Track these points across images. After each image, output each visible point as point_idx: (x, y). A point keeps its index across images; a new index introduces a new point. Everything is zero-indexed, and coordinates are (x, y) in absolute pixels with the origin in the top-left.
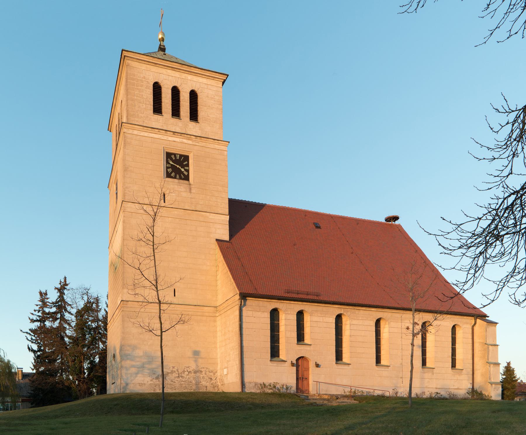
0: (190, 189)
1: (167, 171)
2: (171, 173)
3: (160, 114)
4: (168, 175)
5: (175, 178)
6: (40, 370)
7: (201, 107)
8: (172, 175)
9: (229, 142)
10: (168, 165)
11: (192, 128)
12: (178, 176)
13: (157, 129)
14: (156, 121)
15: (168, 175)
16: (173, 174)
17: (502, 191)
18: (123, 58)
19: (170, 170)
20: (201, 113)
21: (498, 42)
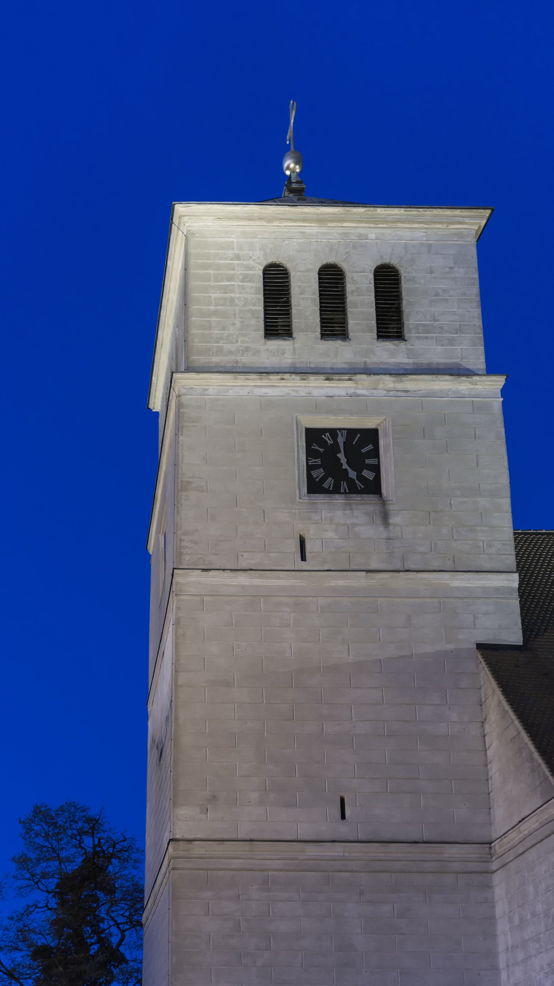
1: (309, 476)
2: (324, 479)
10: (312, 462)
19: (318, 473)
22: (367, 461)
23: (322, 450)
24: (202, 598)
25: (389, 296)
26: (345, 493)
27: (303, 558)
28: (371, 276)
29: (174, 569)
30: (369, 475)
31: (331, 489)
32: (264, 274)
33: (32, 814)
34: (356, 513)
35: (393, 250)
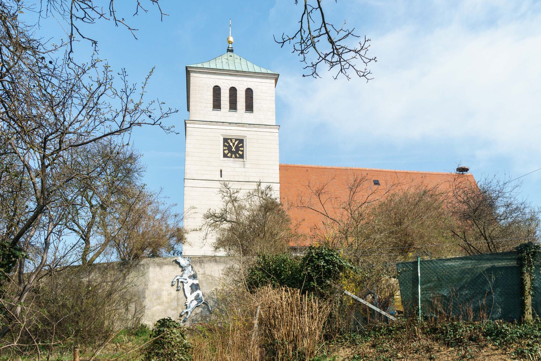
0: (244, 165)
1: (224, 152)
2: (228, 154)
3: (219, 110)
4: (225, 156)
5: (231, 157)
6: (234, 150)
7: (256, 100)
8: (41, 144)
9: (304, 76)
10: (242, 149)
11: (248, 118)
12: (233, 156)
13: (215, 122)
14: (217, 115)
15: (225, 156)
16: (229, 155)
17: (375, 58)
18: (188, 73)
19: (226, 152)
20: (256, 104)
21: (62, 40)
22: (240, 149)
23: (228, 145)
27: (221, 177)
28: (244, 93)
29: (185, 120)
30: (241, 153)
32: (213, 89)
33: (161, 208)
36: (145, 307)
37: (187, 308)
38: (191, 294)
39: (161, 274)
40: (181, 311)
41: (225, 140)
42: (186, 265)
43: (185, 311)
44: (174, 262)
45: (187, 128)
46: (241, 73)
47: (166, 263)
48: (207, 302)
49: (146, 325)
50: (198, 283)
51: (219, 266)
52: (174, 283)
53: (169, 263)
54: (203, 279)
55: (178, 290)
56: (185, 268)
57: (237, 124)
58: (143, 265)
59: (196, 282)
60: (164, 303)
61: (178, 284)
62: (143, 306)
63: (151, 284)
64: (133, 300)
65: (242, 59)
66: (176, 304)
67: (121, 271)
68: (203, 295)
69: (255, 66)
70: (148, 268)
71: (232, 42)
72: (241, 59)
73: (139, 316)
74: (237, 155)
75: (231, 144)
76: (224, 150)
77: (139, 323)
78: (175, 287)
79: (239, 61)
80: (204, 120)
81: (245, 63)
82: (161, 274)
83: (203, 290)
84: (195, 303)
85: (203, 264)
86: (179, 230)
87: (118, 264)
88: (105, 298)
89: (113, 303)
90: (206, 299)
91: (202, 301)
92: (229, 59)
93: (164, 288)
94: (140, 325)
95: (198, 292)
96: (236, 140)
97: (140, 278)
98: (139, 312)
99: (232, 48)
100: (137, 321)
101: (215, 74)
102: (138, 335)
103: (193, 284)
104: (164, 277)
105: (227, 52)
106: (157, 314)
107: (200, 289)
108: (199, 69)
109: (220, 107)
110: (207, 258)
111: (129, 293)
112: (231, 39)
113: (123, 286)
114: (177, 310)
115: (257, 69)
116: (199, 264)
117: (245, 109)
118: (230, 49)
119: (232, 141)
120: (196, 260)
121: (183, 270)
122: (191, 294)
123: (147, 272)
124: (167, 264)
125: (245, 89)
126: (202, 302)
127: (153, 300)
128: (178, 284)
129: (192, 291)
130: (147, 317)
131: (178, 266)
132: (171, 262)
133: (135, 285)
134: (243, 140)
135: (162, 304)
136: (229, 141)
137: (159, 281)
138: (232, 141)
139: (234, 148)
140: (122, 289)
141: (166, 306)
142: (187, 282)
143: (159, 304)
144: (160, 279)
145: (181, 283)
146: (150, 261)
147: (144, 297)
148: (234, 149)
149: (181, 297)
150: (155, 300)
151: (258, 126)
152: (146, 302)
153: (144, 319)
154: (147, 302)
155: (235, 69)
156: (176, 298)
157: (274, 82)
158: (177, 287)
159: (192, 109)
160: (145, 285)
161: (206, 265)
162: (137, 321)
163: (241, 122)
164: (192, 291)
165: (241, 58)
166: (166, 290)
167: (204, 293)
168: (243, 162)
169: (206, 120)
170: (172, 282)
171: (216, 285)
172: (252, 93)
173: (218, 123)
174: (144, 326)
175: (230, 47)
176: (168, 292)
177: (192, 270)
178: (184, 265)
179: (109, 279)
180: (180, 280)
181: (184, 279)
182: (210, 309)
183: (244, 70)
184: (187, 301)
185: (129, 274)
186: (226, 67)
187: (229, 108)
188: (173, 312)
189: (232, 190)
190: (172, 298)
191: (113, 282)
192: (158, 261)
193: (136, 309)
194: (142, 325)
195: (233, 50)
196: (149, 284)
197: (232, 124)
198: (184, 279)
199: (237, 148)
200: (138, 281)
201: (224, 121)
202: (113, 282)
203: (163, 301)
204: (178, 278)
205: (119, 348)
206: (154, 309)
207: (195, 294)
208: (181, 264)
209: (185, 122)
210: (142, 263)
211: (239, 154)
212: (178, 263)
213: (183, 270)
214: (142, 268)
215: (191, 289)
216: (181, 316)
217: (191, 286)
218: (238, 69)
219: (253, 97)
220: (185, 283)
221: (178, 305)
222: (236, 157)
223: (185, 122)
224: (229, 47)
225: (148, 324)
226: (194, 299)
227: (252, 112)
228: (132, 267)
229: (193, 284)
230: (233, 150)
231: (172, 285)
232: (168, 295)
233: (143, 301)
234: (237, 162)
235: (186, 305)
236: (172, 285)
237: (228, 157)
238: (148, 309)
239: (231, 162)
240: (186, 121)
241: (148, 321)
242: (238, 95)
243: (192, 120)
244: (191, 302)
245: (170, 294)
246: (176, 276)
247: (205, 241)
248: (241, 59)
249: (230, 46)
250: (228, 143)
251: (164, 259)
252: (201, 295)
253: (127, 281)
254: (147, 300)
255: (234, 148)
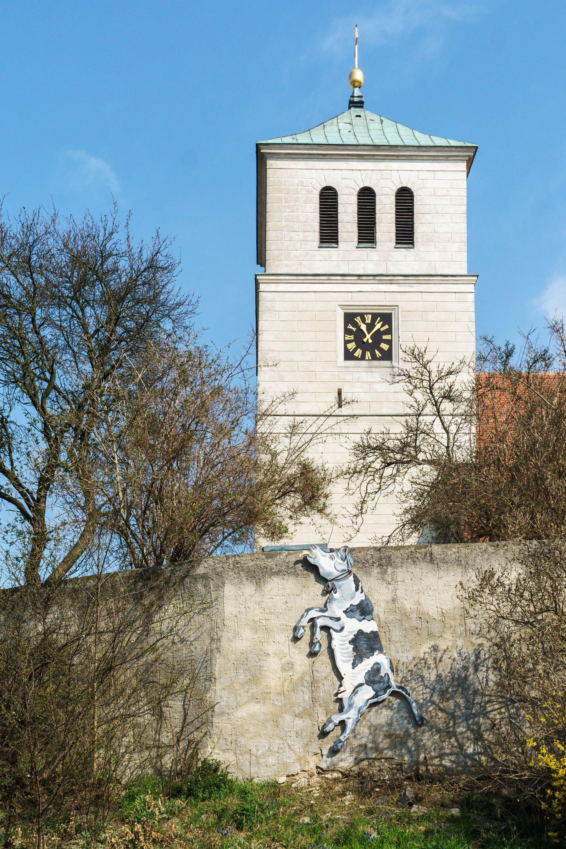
1: (346, 348)
2: (355, 350)
3: (334, 245)
4: (349, 356)
5: (363, 358)
6: (370, 341)
7: (420, 215)
10: (348, 337)
12: (368, 355)
13: (326, 275)
15: (349, 356)
19: (352, 346)
22: (385, 337)
23: (354, 329)
24: (318, 629)
25: (403, 203)
26: (369, 360)
28: (393, 199)
29: (256, 276)
30: (385, 347)
31: (360, 357)
32: (320, 196)
34: (375, 374)
35: (163, 269)
36: (213, 707)
37: (341, 710)
38: (354, 665)
39: (259, 603)
40: (323, 719)
41: (349, 318)
42: (336, 573)
43: (337, 719)
44: (300, 565)
45: (261, 295)
46: (386, 151)
47: (276, 569)
48: (406, 691)
49: (218, 764)
50: (376, 629)
51: (442, 573)
52: (302, 631)
53: (284, 568)
54: (392, 617)
55: (312, 654)
56: (335, 583)
57: (377, 278)
58: (205, 577)
59: (369, 626)
60: (272, 696)
61: (313, 634)
62: (207, 704)
63: (231, 635)
64: (178, 687)
65: (386, 121)
66: (307, 697)
67: (139, 598)
68: (391, 668)
69: (417, 134)
70: (220, 586)
71: (360, 83)
72: (382, 121)
73: (197, 735)
74: (377, 352)
75: (363, 327)
76: (346, 342)
77: (194, 755)
78: (304, 644)
79: (379, 126)
80: (299, 272)
81: (394, 129)
82: (259, 603)
83: (393, 653)
84: (367, 692)
85: (390, 570)
86: (306, 469)
87: (129, 578)
88: (93, 682)
89: (116, 697)
90: (402, 682)
91: (389, 687)
92: (354, 122)
93: (270, 648)
94: (200, 765)
95: (377, 658)
96: (375, 316)
97: (196, 618)
98: (197, 724)
99: (361, 97)
100: (190, 752)
101: (324, 157)
102: (196, 797)
103: (360, 632)
104: (270, 613)
105: (350, 108)
106: (252, 729)
107: (381, 651)
108: (286, 149)
109: (337, 239)
110: (402, 551)
111: (163, 666)
112: (359, 75)
113: (145, 644)
114: (310, 715)
115: (424, 140)
116: (378, 570)
117: (395, 241)
118: (356, 99)
119: (363, 321)
120: (369, 557)
121: (328, 591)
122: (354, 665)
123: (216, 599)
124: (278, 573)
125: (395, 190)
126: (389, 691)
127: (237, 686)
128: (313, 634)
129: (358, 657)
130: (221, 741)
131: (312, 577)
132: (291, 565)
133: (182, 641)
134: (391, 314)
135: (264, 700)
136: (358, 320)
137: (255, 627)
138: (363, 321)
139: (368, 336)
140: (142, 655)
141: (276, 703)
142: (342, 629)
143: (256, 699)
144: (256, 619)
145: (323, 632)
146: (226, 566)
147: (210, 678)
148: (368, 338)
149: (324, 675)
150: (242, 685)
151: (426, 278)
152: (215, 691)
153: (210, 745)
154: (218, 691)
155: (371, 143)
156: (307, 678)
157: (465, 169)
158: (312, 644)
159: (273, 248)
160: (212, 639)
161: (401, 574)
162: (190, 752)
163: (385, 273)
164: (358, 657)
165: (382, 118)
166: (275, 654)
167: (395, 663)
168: (389, 370)
169: (303, 272)
170: (296, 629)
171: (431, 635)
172: (413, 200)
173: (331, 278)
174: (210, 765)
175: (355, 95)
176: (284, 660)
177: (357, 589)
178: (331, 574)
179: (102, 625)
180: (320, 622)
181: (331, 618)
182: (416, 712)
183: (392, 143)
184: (342, 689)
185: (160, 607)
186: (349, 140)
187: (356, 239)
188: (299, 722)
189: (432, 367)
190: (295, 678)
191: (117, 632)
192: (251, 564)
193: (185, 715)
194: (205, 762)
195: (362, 103)
196: (225, 634)
197: (364, 278)
198: (331, 618)
199: (377, 337)
200: (189, 627)
201: (347, 273)
202: (117, 632)
203: (267, 687)
204: (313, 614)
205: (142, 838)
206: (241, 713)
207: (367, 664)
208: (321, 571)
209: (256, 280)
210: (200, 570)
211: (381, 350)
212: (314, 569)
213: (328, 591)
214: (200, 586)
215: (355, 649)
216: (323, 734)
217: (352, 642)
218: (377, 142)
219: (413, 209)
220: (336, 631)
221: (314, 700)
222: (374, 358)
223: (256, 280)
224: (353, 96)
225: (222, 760)
226: (363, 680)
227: (411, 246)
228: (170, 585)
229: (360, 632)
230: (365, 340)
231: (296, 639)
232: (283, 669)
233: (207, 690)
234: (377, 370)
235: (340, 700)
236: (296, 639)
237: (356, 359)
238: (222, 713)
239: (363, 369)
240: (258, 277)
241: (224, 751)
242: (378, 207)
243: (273, 275)
244: (355, 692)
245: (288, 666)
246: (308, 610)
247: (359, 519)
248: (382, 121)
249: (357, 92)
250: (356, 325)
251: (267, 558)
252: (385, 669)
253: (156, 627)
254: (218, 687)
255: (368, 336)
